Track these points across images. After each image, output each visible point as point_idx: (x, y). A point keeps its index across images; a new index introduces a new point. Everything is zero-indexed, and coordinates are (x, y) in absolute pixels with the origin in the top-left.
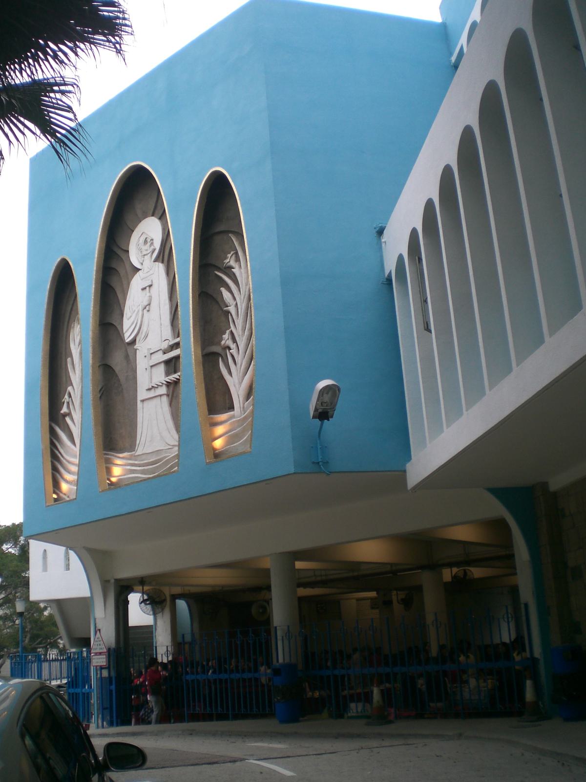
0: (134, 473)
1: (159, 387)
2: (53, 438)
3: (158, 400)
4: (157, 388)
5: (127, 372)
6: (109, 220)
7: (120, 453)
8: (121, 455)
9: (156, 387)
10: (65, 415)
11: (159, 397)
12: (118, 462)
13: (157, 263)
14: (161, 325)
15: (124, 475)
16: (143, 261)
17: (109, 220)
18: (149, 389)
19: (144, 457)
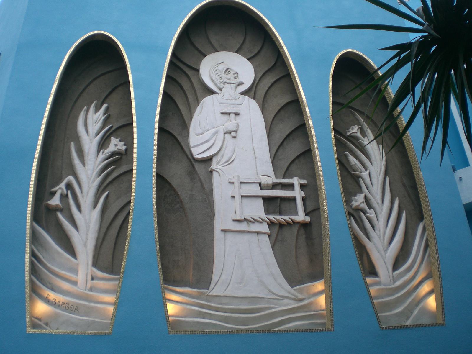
0: (204, 318)
1: (256, 222)
2: (35, 249)
3: (254, 237)
4: (254, 223)
5: (192, 190)
6: (36, 186)
7: (177, 287)
8: (178, 289)
9: (251, 222)
10: (56, 209)
11: (256, 234)
12: (174, 297)
13: (247, 97)
14: (255, 158)
15: (185, 317)
16: (223, 88)
17: (36, 186)
18: (239, 221)
19: (224, 300)
